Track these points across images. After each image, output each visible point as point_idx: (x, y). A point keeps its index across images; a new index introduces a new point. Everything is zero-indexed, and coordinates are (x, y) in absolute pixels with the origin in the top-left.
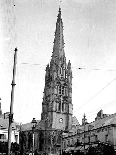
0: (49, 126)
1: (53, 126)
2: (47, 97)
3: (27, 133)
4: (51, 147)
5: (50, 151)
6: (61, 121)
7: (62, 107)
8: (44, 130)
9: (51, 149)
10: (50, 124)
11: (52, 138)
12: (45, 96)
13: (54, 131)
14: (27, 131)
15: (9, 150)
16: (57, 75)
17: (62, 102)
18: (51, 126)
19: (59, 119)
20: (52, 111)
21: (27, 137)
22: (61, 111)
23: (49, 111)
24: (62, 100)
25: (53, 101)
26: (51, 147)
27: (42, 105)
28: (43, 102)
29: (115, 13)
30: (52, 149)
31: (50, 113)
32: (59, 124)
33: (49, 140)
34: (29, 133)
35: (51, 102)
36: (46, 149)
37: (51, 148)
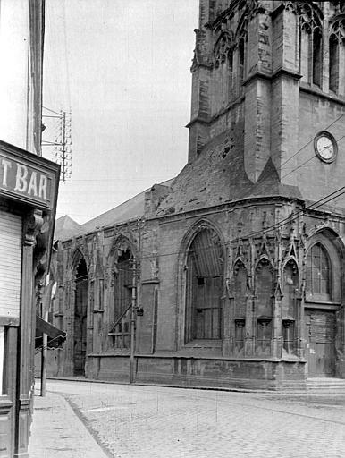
0: (255, 177)
1: (287, 178)
2: (223, 15)
3: (105, 243)
4: (281, 312)
5: (270, 335)
6: (326, 155)
7: (331, 65)
8: (220, 207)
9: (277, 323)
10: (261, 164)
11: (282, 249)
12: (211, 14)
13: (289, 209)
14: (107, 230)
15: (33, 142)
16: (75, 410)
17: (327, 31)
18: (271, 171)
19: (316, 139)
20: (273, 79)
21: (109, 264)
22: (326, 85)
23: (258, 76)
24: (327, 18)
25: (276, 15)
26: (281, 312)
27: (193, 70)
28: (197, 50)
29: (285, 193)
30: (286, 323)
31: (260, 89)
32: (318, 168)
33: (265, 263)
34: (116, 242)
35: (262, 19)
36: (241, 323)
37: (277, 313)
